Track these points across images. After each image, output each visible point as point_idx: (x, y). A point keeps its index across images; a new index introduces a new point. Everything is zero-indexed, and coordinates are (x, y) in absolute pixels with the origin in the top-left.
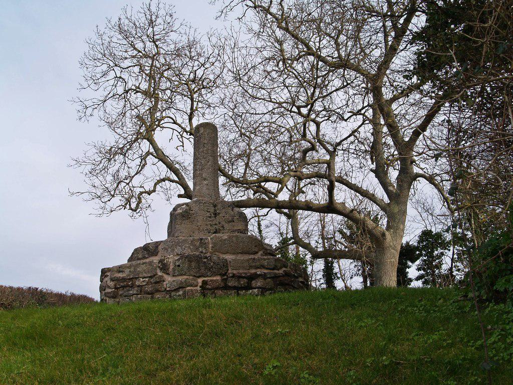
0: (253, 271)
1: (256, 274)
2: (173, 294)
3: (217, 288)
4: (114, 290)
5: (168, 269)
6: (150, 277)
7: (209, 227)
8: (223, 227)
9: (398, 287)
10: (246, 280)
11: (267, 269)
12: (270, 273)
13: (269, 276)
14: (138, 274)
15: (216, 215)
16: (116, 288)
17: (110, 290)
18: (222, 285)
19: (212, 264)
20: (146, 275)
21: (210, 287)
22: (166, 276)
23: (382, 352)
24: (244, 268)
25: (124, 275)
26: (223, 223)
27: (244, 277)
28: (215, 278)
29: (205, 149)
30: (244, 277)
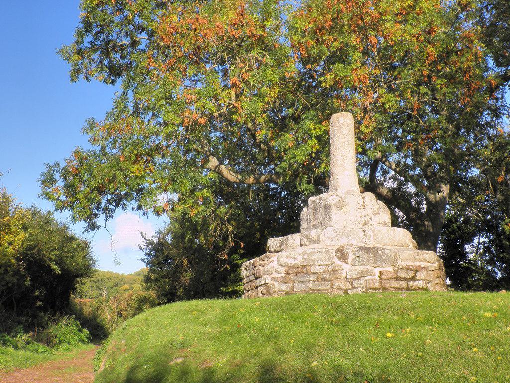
0: (417, 264)
1: (420, 266)
2: (355, 282)
3: (392, 279)
4: (285, 275)
5: (347, 259)
6: (326, 265)
7: (359, 218)
8: (370, 219)
9: (295, 194)
10: (413, 272)
11: (429, 262)
12: (431, 266)
13: (430, 269)
14: (314, 262)
15: (364, 207)
16: (288, 274)
17: (279, 275)
18: (395, 276)
19: (386, 256)
20: (322, 263)
21: (386, 277)
22: (344, 265)
23: (487, 213)
24: (410, 261)
25: (296, 262)
26: (371, 215)
27: (411, 270)
28: (14, 300)
29: (346, 139)
30: (411, 270)
